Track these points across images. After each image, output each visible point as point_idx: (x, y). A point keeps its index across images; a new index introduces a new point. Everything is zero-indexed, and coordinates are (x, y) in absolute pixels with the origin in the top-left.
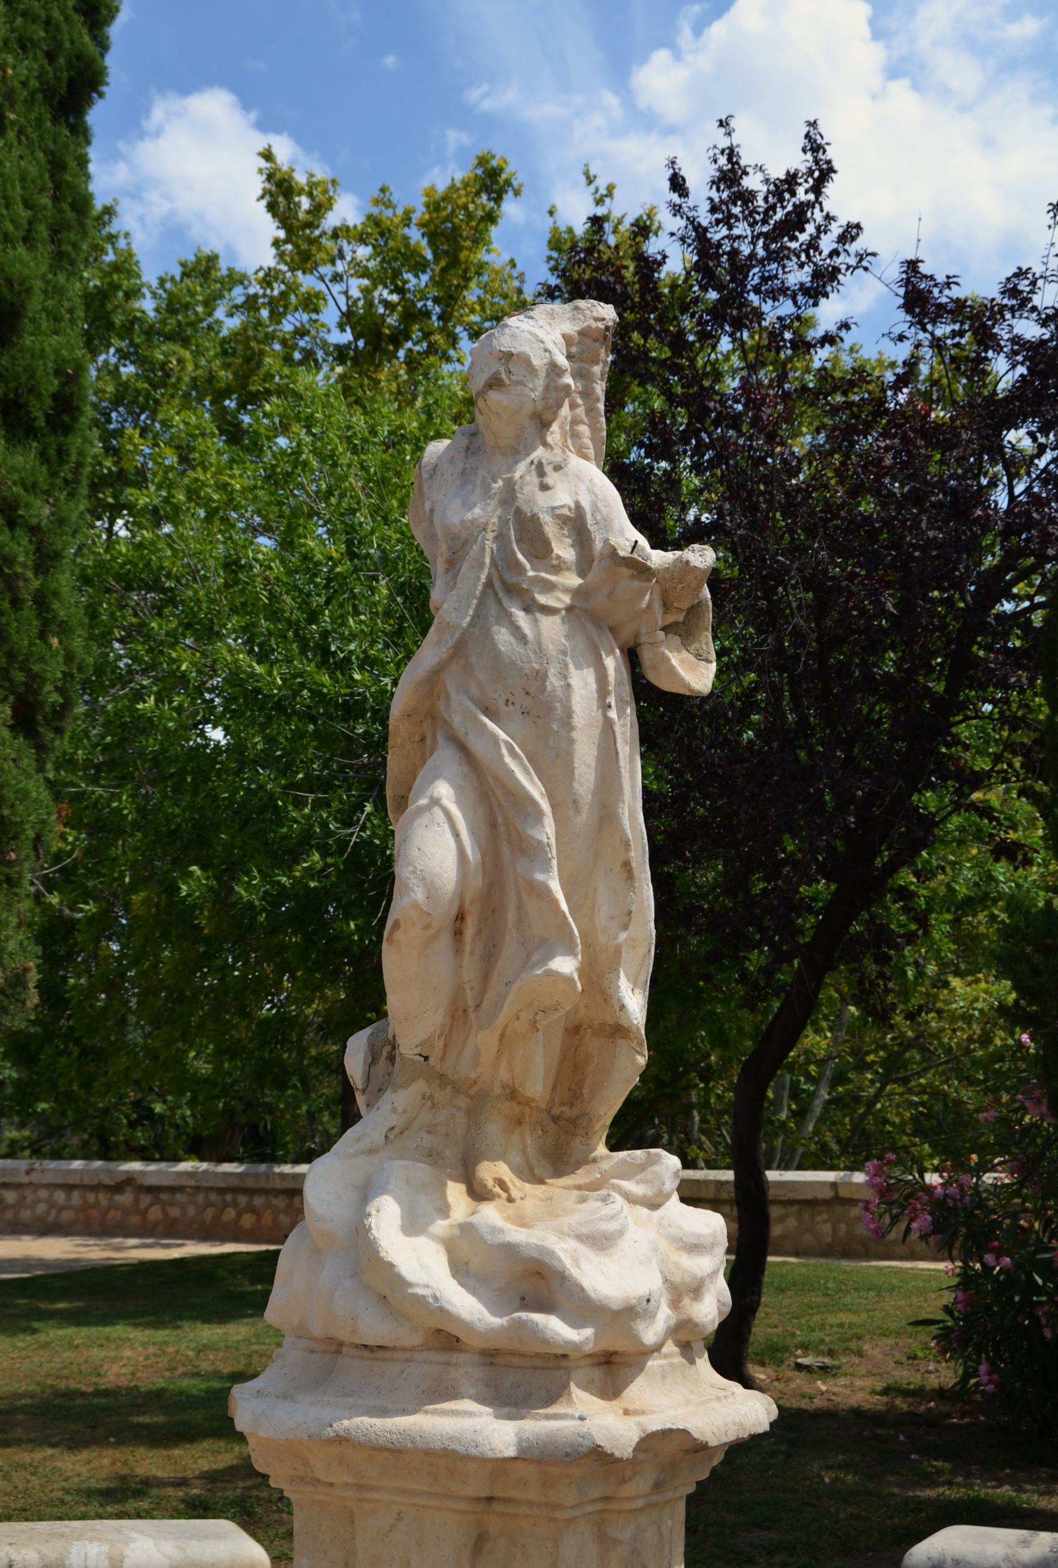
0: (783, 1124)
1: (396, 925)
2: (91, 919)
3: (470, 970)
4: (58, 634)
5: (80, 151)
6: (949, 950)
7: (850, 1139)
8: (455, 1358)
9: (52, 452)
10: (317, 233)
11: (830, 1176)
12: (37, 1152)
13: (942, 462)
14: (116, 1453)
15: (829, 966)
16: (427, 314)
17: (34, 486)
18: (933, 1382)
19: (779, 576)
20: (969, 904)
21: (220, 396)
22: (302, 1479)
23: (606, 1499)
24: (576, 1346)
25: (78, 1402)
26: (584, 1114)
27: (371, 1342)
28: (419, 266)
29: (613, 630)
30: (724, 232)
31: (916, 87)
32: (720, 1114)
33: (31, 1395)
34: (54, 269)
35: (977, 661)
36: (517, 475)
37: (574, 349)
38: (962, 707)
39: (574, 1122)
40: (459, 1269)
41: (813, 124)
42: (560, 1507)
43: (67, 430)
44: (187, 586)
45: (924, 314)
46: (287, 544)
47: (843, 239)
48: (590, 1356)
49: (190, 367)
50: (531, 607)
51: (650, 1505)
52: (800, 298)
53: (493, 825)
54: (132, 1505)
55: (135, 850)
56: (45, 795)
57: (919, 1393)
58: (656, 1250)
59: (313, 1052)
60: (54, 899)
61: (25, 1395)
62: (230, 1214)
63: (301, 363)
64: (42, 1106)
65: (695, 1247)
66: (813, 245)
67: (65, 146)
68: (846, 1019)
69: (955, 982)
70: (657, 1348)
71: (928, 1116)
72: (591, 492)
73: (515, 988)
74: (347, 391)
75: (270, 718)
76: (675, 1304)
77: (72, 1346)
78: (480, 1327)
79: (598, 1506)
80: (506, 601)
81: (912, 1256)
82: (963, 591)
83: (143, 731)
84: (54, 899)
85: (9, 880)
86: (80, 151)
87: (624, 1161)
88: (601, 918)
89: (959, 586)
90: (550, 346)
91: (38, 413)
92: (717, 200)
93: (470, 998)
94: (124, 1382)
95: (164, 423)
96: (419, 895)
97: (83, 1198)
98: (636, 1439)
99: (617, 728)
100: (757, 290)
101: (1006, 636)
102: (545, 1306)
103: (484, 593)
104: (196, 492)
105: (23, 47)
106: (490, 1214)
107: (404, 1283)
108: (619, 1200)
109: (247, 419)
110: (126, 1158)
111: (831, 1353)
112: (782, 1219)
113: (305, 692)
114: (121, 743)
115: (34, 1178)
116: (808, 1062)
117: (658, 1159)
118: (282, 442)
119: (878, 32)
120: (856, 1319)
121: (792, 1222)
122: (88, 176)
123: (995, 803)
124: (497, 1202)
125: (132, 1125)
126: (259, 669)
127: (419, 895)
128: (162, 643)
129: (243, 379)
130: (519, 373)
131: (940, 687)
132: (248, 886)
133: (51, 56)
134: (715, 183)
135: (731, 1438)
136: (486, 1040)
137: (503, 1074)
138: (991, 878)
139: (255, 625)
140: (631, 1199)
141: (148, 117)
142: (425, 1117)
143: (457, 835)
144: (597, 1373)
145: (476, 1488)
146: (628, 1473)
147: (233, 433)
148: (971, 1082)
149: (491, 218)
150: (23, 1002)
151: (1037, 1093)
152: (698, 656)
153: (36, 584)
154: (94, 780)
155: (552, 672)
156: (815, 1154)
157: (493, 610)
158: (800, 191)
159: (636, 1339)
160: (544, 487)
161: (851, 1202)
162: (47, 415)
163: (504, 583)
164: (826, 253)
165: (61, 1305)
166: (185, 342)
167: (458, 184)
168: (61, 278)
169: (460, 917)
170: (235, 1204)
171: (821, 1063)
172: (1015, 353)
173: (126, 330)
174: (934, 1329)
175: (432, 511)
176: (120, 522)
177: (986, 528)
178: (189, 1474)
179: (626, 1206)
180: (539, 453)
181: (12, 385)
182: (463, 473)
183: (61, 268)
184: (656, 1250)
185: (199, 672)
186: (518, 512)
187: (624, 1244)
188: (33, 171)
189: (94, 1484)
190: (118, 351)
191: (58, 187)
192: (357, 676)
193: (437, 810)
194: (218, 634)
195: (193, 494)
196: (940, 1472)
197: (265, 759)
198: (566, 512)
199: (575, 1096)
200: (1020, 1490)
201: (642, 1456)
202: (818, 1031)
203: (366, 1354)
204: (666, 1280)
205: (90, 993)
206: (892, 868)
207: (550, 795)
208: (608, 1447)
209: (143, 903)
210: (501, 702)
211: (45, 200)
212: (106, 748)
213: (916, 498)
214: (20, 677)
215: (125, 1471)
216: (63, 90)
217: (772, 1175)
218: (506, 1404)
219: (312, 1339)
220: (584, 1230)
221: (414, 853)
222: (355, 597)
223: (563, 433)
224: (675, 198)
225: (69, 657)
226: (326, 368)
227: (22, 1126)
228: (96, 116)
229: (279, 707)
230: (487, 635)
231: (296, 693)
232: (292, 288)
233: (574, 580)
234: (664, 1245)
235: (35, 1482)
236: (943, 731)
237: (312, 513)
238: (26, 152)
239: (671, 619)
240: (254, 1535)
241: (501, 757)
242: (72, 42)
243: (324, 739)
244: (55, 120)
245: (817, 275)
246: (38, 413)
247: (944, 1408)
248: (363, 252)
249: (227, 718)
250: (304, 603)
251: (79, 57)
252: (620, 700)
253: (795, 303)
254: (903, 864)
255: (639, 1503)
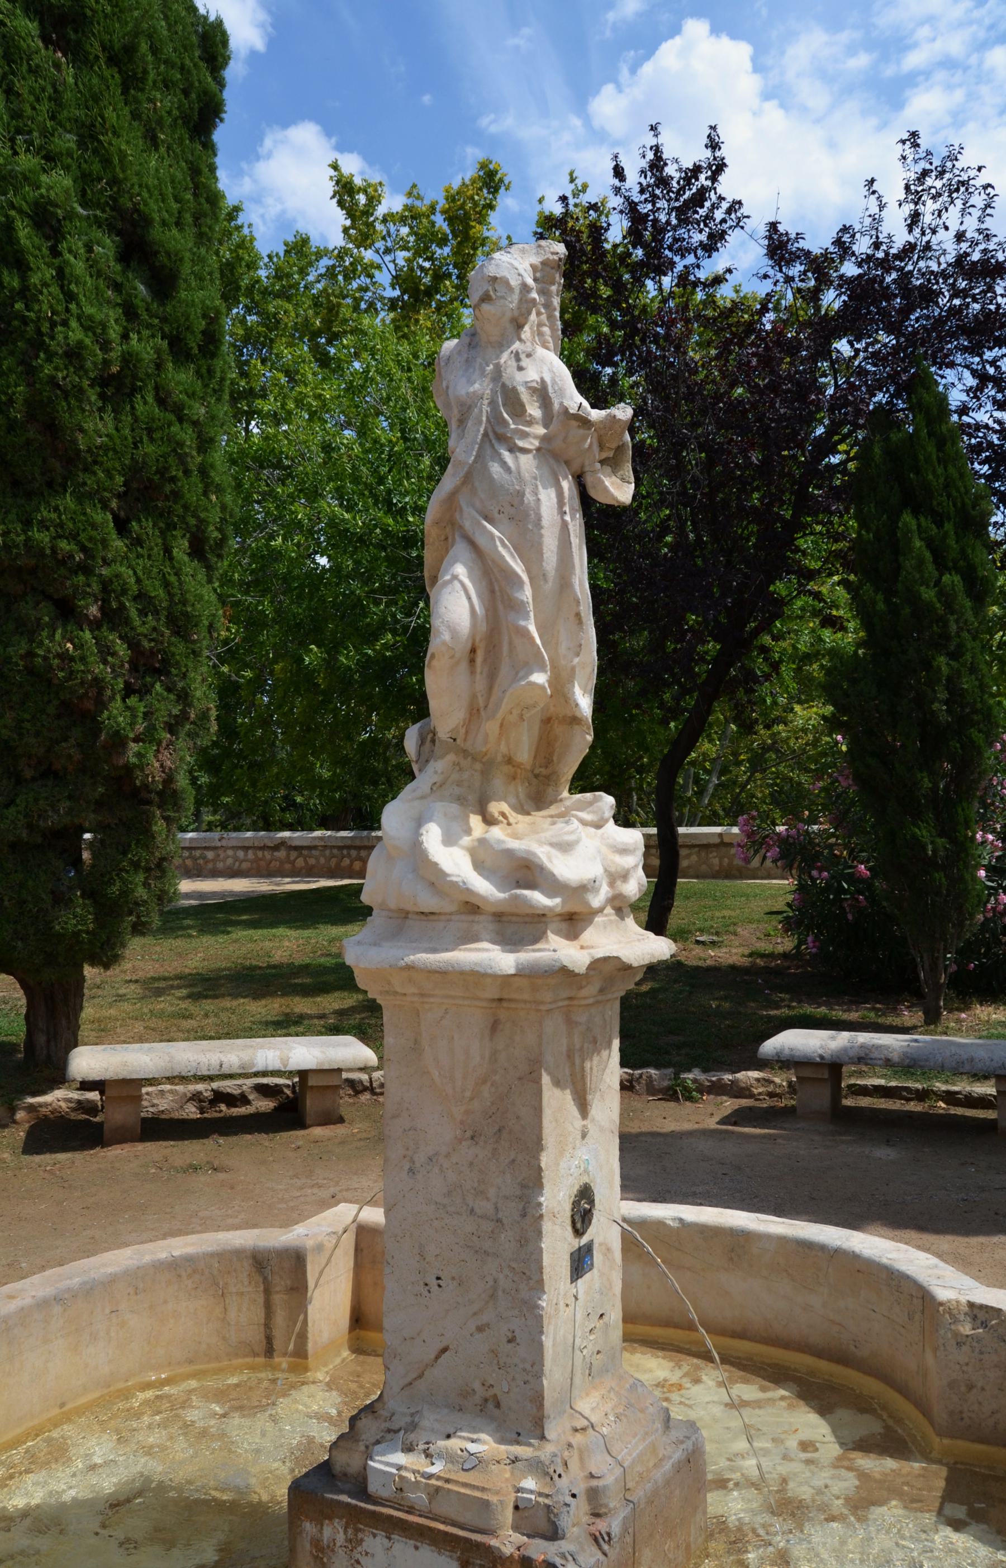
0: (689, 799)
1: (433, 656)
2: (250, 681)
3: (481, 684)
4: (215, 493)
5: (210, 161)
6: (793, 686)
7: (731, 808)
8: (477, 918)
9: (204, 370)
10: (372, 219)
11: (718, 830)
12: (224, 826)
13: (791, 364)
14: (283, 1001)
15: (714, 697)
16: (450, 275)
17: (194, 394)
18: (780, 949)
19: (683, 444)
20: (807, 658)
21: (315, 334)
22: (387, 992)
23: (570, 998)
24: (551, 909)
25: (258, 972)
26: (554, 773)
27: (426, 910)
28: (443, 242)
29: (567, 463)
30: (649, 206)
31: (783, 106)
32: (650, 794)
33: (229, 969)
34: (198, 244)
35: (813, 496)
36: (502, 361)
37: (538, 275)
38: (804, 526)
39: (548, 777)
40: (479, 866)
41: (713, 128)
42: (542, 1003)
43: (213, 355)
44: (299, 464)
45: (782, 258)
46: (363, 432)
47: (729, 211)
48: (560, 915)
49: (293, 314)
50: (513, 449)
51: (598, 1002)
52: (699, 252)
53: (492, 592)
54: (293, 1029)
55: (275, 636)
56: (213, 598)
57: (771, 956)
58: (599, 852)
59: (394, 762)
60: (225, 669)
61: (225, 969)
62: (346, 862)
63: (366, 311)
64: (226, 800)
65: (624, 851)
66: (709, 217)
67: (200, 157)
68: (729, 732)
69: (797, 708)
70: (601, 910)
71: (780, 793)
72: (551, 371)
73: (508, 694)
74: (397, 328)
75: (356, 548)
76: (612, 884)
77: (252, 940)
78: (491, 899)
79: (566, 1003)
80: (496, 445)
81: (769, 877)
82: (803, 450)
83: (276, 560)
84: (225, 669)
85: (194, 652)
86: (210, 161)
87: (579, 800)
88: (563, 649)
89: (801, 446)
90: (522, 272)
91: (193, 343)
92: (645, 184)
93: (481, 702)
94: (285, 960)
95: (277, 355)
96: (446, 636)
97: (255, 854)
98: (588, 962)
99: (570, 527)
100: (670, 248)
101: (831, 478)
102: (532, 886)
103: (482, 440)
104: (302, 401)
105: (166, 86)
106: (496, 833)
107: (445, 875)
108: (576, 823)
109: (333, 351)
110: (281, 830)
111: (717, 934)
112: (688, 856)
113: (378, 531)
114: (262, 568)
115: (224, 843)
116: (705, 761)
117: (601, 797)
118: (357, 365)
119: (758, 67)
120: (733, 914)
121: (694, 858)
122: (217, 179)
123: (824, 590)
124: (501, 826)
125: (283, 810)
126: (347, 516)
127: (446, 636)
128: (285, 502)
129: (328, 323)
130: (501, 290)
131: (788, 514)
132: (347, 657)
133: (186, 93)
134: (643, 172)
135: (647, 962)
136: (491, 727)
137: (503, 748)
138: (820, 640)
139: (343, 487)
140: (584, 823)
141: (261, 146)
142: (455, 776)
143: (469, 598)
144: (564, 926)
145: (493, 993)
146: (584, 983)
147: (324, 360)
148: (807, 770)
149: (491, 207)
150: (208, 729)
151: (846, 772)
152: (623, 480)
153: (199, 459)
154: (247, 593)
155: (528, 491)
156: (709, 817)
157: (489, 451)
158: (702, 177)
159: (587, 904)
160: (520, 369)
161: (730, 845)
162: (199, 346)
163: (495, 433)
164: (718, 221)
165: (244, 917)
166: (289, 299)
167: (467, 182)
168: (203, 251)
169: (473, 650)
170: (349, 856)
171: (713, 761)
172: (840, 286)
173: (250, 291)
174: (780, 917)
175: (447, 387)
176: (253, 423)
177: (819, 409)
178: (327, 1012)
179: (580, 826)
180: (517, 346)
181: (175, 325)
182: (467, 361)
183: (202, 244)
184: (599, 852)
185: (310, 520)
186: (504, 385)
187: (580, 849)
188: (179, 175)
189: (269, 1018)
190: (246, 306)
191: (196, 187)
192: (411, 519)
193: (456, 582)
194: (321, 495)
195: (299, 402)
196: (782, 1000)
197: (355, 574)
198: (534, 384)
199: (548, 762)
200: (832, 1009)
201: (592, 973)
202: (711, 741)
203: (423, 917)
204: (606, 870)
205: (252, 728)
206: (756, 632)
207: (528, 571)
208: (571, 967)
209: (282, 669)
210: (496, 511)
211: (189, 196)
212: (252, 572)
213: (774, 387)
214: (193, 521)
215: (288, 1011)
216: (196, 116)
217: (681, 830)
218: (507, 944)
219: (390, 910)
220: (554, 840)
221: (443, 610)
222: (407, 467)
223: (533, 333)
224: (617, 182)
225: (224, 508)
226: (382, 314)
227: (215, 813)
228: (220, 135)
229: (361, 539)
230: (486, 468)
231: (371, 531)
232: (357, 261)
233: (541, 431)
234: (604, 850)
235: (234, 1018)
236: (789, 543)
237: (379, 413)
238: (173, 162)
239: (604, 455)
240: (368, 1045)
241: (496, 547)
242: (200, 82)
243: (391, 561)
244: (192, 139)
245: (711, 236)
246: (193, 343)
247: (786, 964)
248: (405, 231)
249: (332, 551)
250: (375, 472)
251: (206, 93)
252: (572, 509)
253: (696, 256)
254: (763, 630)
255: (591, 1001)
